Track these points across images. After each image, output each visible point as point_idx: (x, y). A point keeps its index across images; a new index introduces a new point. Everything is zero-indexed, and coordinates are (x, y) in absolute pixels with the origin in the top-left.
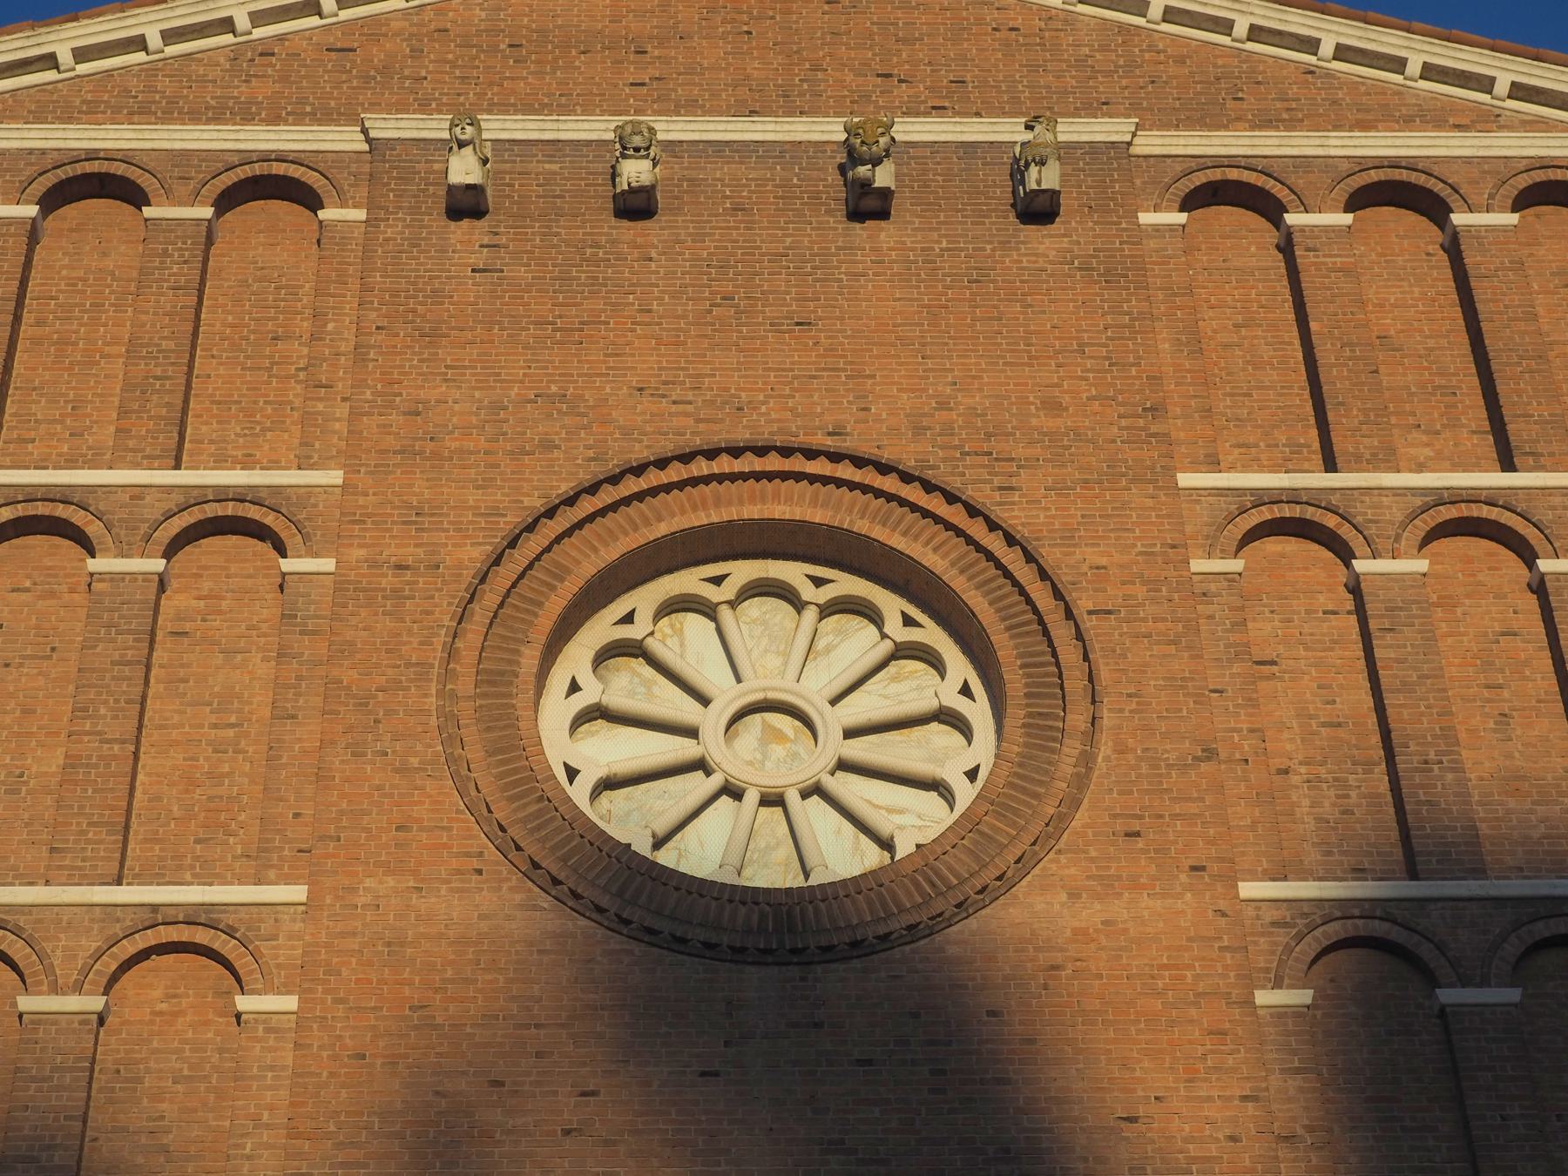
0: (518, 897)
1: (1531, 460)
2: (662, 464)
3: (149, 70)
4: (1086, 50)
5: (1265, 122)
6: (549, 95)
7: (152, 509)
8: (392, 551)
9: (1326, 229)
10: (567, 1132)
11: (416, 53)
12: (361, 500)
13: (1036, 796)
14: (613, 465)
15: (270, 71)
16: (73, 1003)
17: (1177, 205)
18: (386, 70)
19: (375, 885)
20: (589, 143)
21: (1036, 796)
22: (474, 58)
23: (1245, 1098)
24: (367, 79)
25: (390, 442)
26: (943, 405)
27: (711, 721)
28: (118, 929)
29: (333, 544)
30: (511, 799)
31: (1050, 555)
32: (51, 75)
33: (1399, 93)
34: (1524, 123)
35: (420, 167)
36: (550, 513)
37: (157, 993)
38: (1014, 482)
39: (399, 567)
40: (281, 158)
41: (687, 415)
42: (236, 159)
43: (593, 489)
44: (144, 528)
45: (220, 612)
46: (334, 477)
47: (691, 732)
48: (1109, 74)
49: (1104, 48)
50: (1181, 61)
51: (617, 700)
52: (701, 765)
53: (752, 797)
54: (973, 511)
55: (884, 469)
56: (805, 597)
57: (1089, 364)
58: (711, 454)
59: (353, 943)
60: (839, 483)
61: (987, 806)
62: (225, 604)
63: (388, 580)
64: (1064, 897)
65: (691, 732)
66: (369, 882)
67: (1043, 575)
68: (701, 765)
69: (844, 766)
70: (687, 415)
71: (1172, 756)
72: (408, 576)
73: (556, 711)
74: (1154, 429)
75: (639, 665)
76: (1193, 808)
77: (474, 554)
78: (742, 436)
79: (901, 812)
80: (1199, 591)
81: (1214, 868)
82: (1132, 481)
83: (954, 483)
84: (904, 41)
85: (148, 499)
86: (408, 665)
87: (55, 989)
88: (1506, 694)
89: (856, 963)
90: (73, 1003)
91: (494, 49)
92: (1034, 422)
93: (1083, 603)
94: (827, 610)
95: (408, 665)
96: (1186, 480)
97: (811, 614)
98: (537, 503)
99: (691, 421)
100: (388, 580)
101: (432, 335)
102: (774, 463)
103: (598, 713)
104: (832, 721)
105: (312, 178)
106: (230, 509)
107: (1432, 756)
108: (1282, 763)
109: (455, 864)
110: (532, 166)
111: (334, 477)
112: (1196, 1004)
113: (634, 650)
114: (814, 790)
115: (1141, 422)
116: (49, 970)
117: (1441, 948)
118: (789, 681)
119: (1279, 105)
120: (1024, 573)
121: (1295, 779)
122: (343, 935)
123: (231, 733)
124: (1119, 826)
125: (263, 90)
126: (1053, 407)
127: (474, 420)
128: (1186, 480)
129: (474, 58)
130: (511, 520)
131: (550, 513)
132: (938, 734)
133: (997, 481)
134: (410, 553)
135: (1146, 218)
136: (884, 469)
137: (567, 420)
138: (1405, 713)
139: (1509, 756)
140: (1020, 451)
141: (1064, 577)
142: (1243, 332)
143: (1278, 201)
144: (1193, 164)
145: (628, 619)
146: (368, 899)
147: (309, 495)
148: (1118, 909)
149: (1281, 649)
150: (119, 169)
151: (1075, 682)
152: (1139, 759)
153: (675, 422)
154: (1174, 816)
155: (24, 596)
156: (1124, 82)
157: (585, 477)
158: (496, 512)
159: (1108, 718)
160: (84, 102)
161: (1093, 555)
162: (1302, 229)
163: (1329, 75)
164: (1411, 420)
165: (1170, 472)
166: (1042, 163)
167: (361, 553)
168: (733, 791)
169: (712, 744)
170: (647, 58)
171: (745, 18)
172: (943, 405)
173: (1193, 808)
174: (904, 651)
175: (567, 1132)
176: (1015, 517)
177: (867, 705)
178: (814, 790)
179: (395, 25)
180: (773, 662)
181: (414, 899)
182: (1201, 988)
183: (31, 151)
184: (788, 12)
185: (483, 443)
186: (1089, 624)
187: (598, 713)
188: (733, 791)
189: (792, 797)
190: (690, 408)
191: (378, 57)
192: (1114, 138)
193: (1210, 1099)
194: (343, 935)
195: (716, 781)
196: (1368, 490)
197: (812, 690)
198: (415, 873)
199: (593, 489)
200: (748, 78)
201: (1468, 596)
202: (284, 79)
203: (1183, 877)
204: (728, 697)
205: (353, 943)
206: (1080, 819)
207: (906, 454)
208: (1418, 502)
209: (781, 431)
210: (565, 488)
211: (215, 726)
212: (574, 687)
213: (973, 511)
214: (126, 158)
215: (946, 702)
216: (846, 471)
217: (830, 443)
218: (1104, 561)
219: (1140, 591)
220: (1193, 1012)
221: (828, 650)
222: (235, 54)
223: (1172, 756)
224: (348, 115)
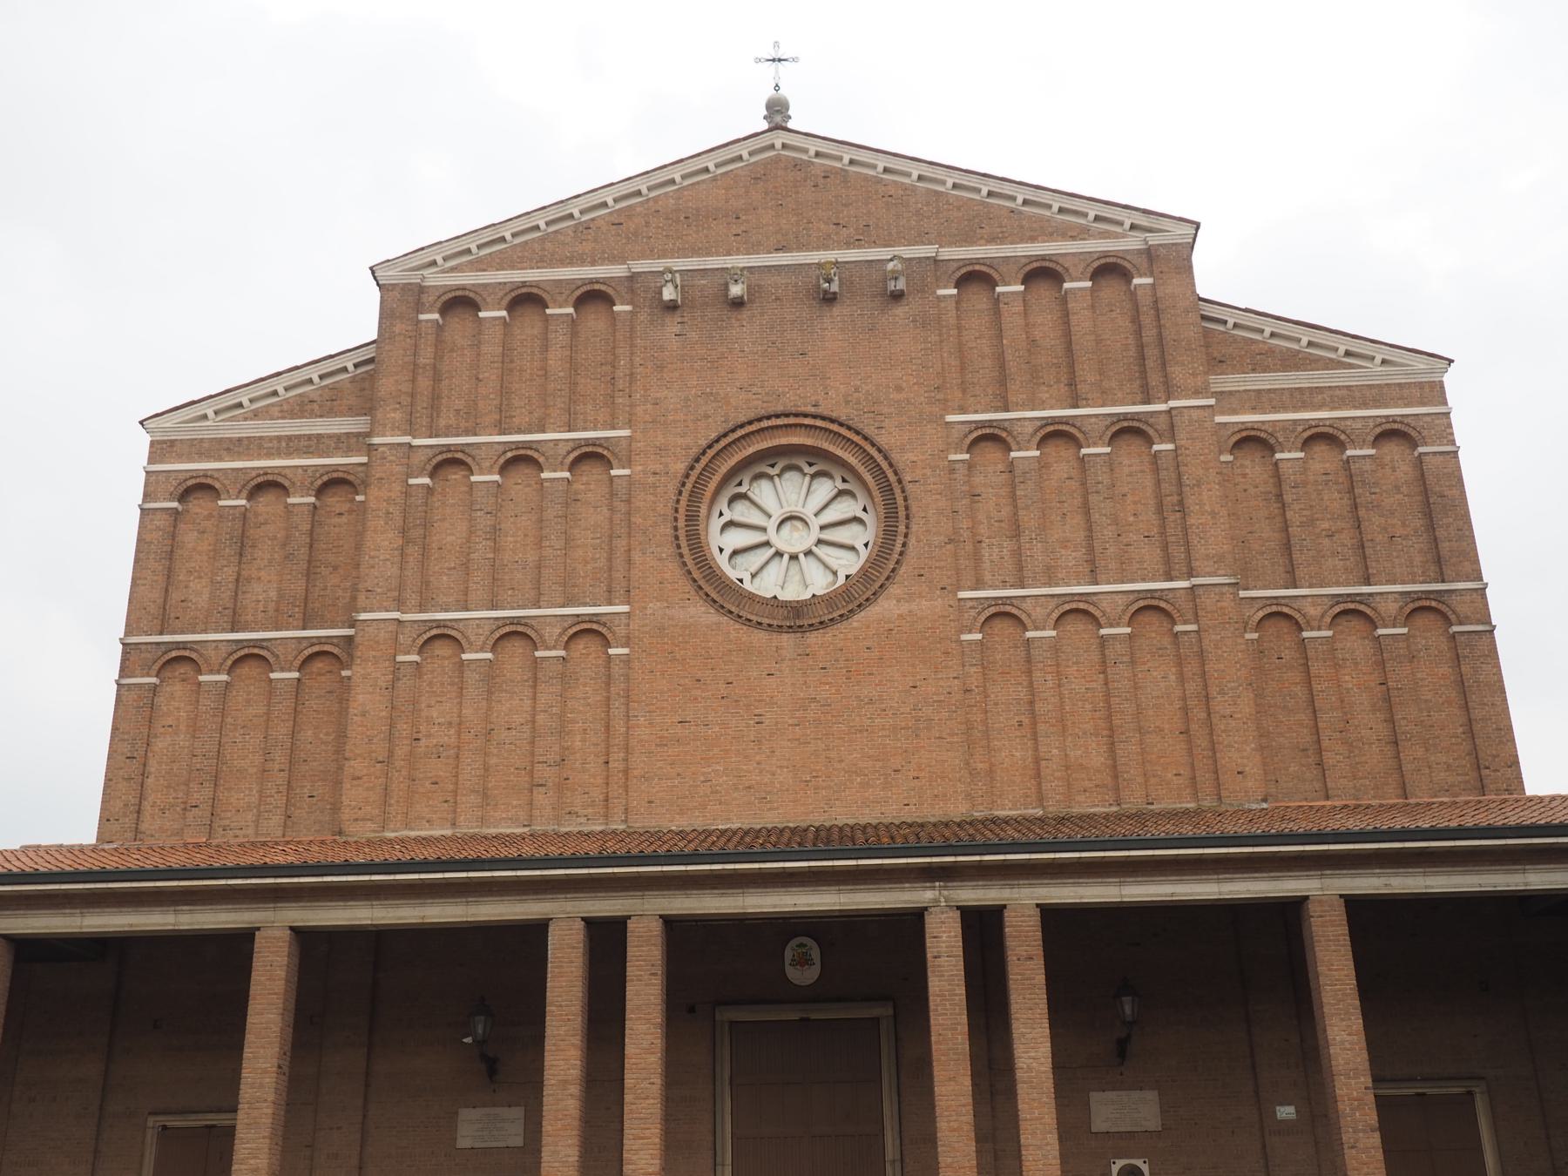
0: (703, 609)
1: (1084, 402)
2: (750, 423)
3: (542, 240)
4: (920, 205)
5: (992, 240)
6: (701, 242)
7: (563, 449)
8: (652, 467)
9: (1013, 293)
10: (723, 698)
11: (647, 224)
12: (639, 445)
13: (887, 559)
14: (731, 425)
15: (589, 237)
16: (553, 653)
17: (953, 285)
18: (636, 234)
19: (653, 606)
20: (718, 269)
21: (887, 559)
22: (671, 225)
23: (954, 678)
24: (628, 238)
25: (648, 418)
26: (857, 390)
27: (771, 525)
28: (566, 625)
29: (628, 463)
30: (699, 568)
31: (895, 456)
32: (504, 246)
33: (1048, 221)
34: (1100, 233)
35: (653, 285)
36: (710, 446)
37: (581, 646)
38: (883, 425)
39: (655, 473)
40: (597, 281)
41: (758, 399)
42: (580, 283)
43: (725, 435)
44: (560, 458)
45: (590, 490)
46: (626, 433)
47: (764, 530)
48: (928, 218)
49: (928, 204)
50: (959, 209)
51: (737, 518)
52: (767, 544)
53: (786, 557)
54: (866, 438)
55: (832, 421)
56: (806, 471)
57: (914, 367)
58: (769, 418)
59: (647, 629)
60: (816, 427)
61: (869, 565)
62: (592, 487)
63: (651, 479)
64: (895, 602)
65: (764, 530)
66: (651, 605)
67: (891, 465)
68: (767, 544)
69: (820, 542)
70: (758, 399)
71: (936, 543)
72: (658, 477)
73: (716, 523)
74: (937, 397)
75: (747, 503)
76: (943, 564)
77: (681, 467)
78: (780, 409)
79: (840, 558)
80: (952, 468)
81: (949, 588)
82: (928, 422)
83: (860, 426)
84: (845, 205)
85: (560, 446)
86: (660, 515)
87: (548, 648)
88: (1066, 505)
89: (821, 631)
90: (553, 653)
91: (677, 221)
92: (892, 396)
93: (907, 478)
94: (814, 476)
95: (660, 515)
96: (950, 418)
97: (807, 479)
98: (704, 443)
99: (760, 402)
100: (651, 479)
101: (661, 368)
102: (792, 420)
103: (731, 524)
104: (815, 523)
105: (610, 291)
106: (590, 449)
107: (1034, 537)
108: (979, 538)
109: (681, 596)
110: (696, 282)
111: (626, 433)
112: (940, 643)
113: (744, 496)
114: (820, 542)
115: (933, 394)
116: (544, 641)
117: (1029, 616)
118: (799, 508)
119: (998, 230)
120: (884, 465)
121: (984, 545)
122: (643, 626)
123: (598, 541)
124: (916, 574)
125: (587, 247)
126: (899, 389)
127: (679, 406)
128: (950, 418)
129: (671, 225)
130: (695, 451)
131: (710, 446)
132: (855, 528)
133: (877, 425)
134: (658, 468)
135: (941, 292)
136: (832, 421)
137: (714, 405)
138: (1026, 519)
139: (1065, 532)
140: (885, 410)
141: (900, 466)
142: (978, 341)
143: (995, 280)
144: (961, 263)
145: (740, 484)
146: (651, 611)
147: (619, 441)
148: (914, 606)
149: (983, 489)
150: (535, 290)
151: (902, 513)
152: (925, 544)
153: (756, 402)
154: (936, 568)
155: (520, 487)
156: (935, 222)
157: (721, 431)
158: (688, 448)
159: (914, 528)
160: (518, 257)
161: (910, 456)
162: (1003, 293)
163: (1021, 212)
164: (1042, 380)
165: (942, 417)
166: (896, 279)
167: (640, 468)
168: (779, 554)
169: (772, 535)
170: (740, 221)
171: (780, 197)
172: (857, 390)
173: (943, 564)
174: (841, 493)
175: (723, 698)
176: (882, 440)
177: (830, 516)
178: (808, 553)
179: (638, 209)
180: (794, 497)
181: (667, 611)
182: (942, 636)
183: (500, 283)
184: (797, 193)
185: (683, 418)
186: (909, 487)
187: (731, 524)
188: (779, 554)
189: (815, 549)
190: (760, 396)
191: (632, 227)
192: (929, 255)
193: (942, 678)
194: (643, 626)
195: (772, 551)
196: (1019, 419)
197: (808, 511)
198: (667, 601)
199: (725, 435)
200: (781, 229)
201: (1056, 462)
202: (595, 241)
203: (938, 592)
204: (777, 515)
205: (647, 629)
206: (902, 570)
207: (842, 413)
208: (1039, 423)
209: (795, 406)
210: (713, 436)
211: (593, 539)
212: (721, 514)
213: (866, 438)
214: (537, 285)
215: (858, 515)
216: (819, 423)
217: (812, 410)
218: (915, 459)
219: (928, 472)
220: (938, 645)
221: (815, 491)
222: (576, 228)
223: (936, 543)
224: (622, 259)
